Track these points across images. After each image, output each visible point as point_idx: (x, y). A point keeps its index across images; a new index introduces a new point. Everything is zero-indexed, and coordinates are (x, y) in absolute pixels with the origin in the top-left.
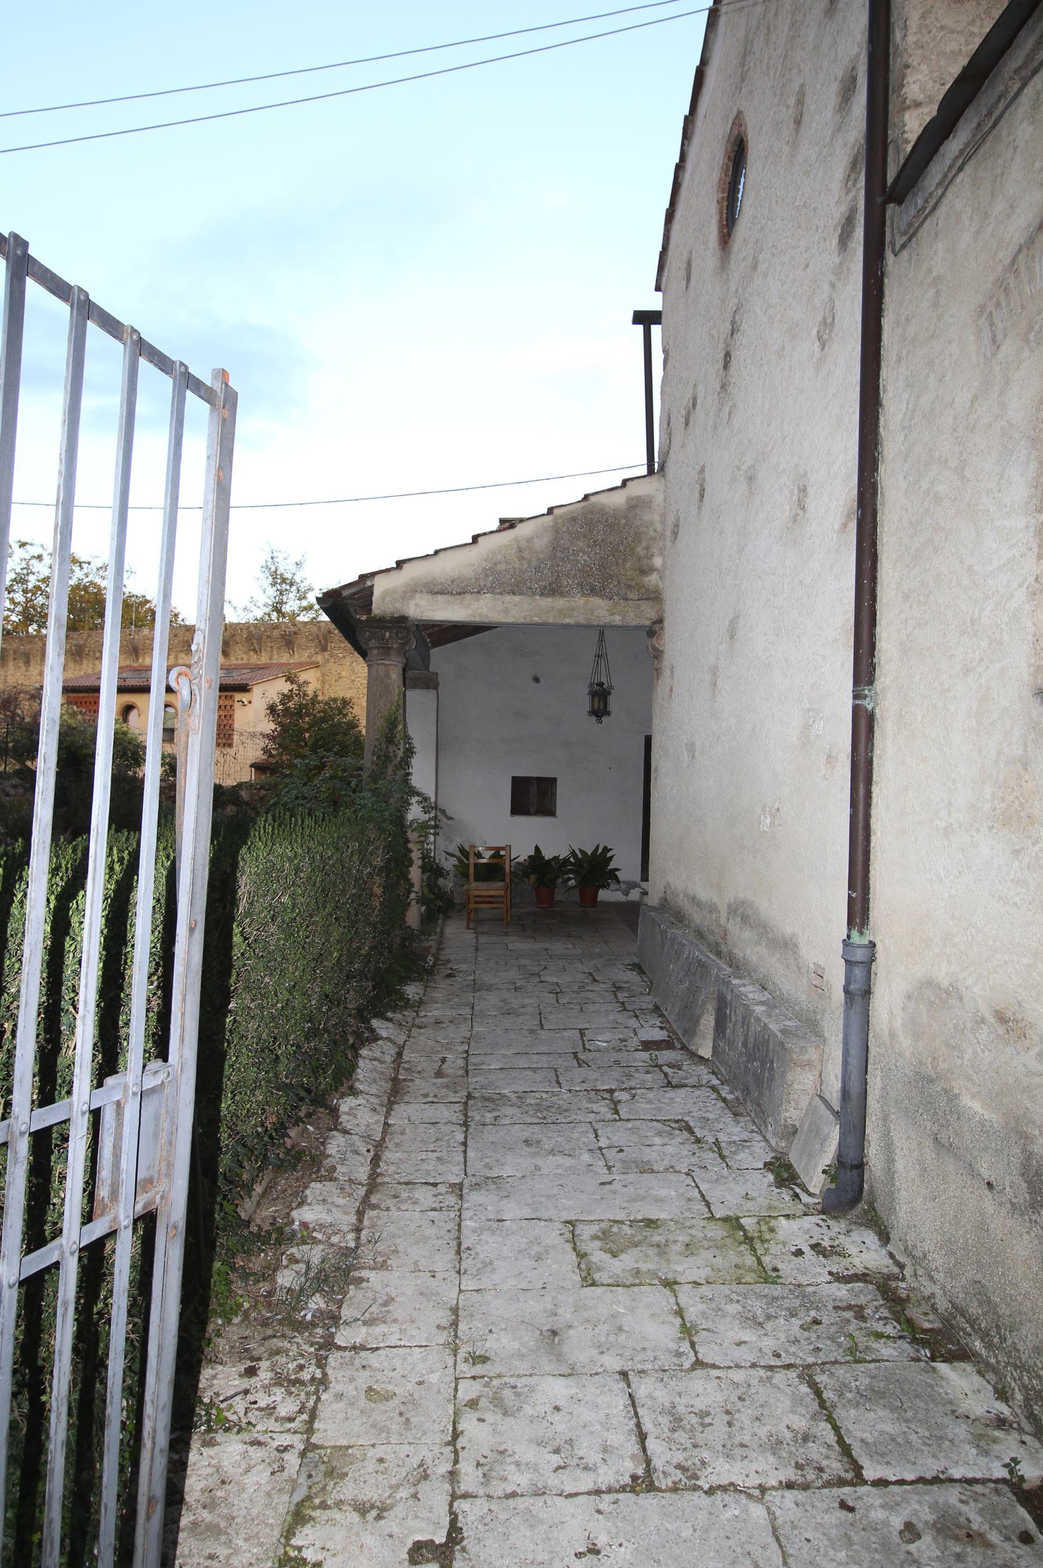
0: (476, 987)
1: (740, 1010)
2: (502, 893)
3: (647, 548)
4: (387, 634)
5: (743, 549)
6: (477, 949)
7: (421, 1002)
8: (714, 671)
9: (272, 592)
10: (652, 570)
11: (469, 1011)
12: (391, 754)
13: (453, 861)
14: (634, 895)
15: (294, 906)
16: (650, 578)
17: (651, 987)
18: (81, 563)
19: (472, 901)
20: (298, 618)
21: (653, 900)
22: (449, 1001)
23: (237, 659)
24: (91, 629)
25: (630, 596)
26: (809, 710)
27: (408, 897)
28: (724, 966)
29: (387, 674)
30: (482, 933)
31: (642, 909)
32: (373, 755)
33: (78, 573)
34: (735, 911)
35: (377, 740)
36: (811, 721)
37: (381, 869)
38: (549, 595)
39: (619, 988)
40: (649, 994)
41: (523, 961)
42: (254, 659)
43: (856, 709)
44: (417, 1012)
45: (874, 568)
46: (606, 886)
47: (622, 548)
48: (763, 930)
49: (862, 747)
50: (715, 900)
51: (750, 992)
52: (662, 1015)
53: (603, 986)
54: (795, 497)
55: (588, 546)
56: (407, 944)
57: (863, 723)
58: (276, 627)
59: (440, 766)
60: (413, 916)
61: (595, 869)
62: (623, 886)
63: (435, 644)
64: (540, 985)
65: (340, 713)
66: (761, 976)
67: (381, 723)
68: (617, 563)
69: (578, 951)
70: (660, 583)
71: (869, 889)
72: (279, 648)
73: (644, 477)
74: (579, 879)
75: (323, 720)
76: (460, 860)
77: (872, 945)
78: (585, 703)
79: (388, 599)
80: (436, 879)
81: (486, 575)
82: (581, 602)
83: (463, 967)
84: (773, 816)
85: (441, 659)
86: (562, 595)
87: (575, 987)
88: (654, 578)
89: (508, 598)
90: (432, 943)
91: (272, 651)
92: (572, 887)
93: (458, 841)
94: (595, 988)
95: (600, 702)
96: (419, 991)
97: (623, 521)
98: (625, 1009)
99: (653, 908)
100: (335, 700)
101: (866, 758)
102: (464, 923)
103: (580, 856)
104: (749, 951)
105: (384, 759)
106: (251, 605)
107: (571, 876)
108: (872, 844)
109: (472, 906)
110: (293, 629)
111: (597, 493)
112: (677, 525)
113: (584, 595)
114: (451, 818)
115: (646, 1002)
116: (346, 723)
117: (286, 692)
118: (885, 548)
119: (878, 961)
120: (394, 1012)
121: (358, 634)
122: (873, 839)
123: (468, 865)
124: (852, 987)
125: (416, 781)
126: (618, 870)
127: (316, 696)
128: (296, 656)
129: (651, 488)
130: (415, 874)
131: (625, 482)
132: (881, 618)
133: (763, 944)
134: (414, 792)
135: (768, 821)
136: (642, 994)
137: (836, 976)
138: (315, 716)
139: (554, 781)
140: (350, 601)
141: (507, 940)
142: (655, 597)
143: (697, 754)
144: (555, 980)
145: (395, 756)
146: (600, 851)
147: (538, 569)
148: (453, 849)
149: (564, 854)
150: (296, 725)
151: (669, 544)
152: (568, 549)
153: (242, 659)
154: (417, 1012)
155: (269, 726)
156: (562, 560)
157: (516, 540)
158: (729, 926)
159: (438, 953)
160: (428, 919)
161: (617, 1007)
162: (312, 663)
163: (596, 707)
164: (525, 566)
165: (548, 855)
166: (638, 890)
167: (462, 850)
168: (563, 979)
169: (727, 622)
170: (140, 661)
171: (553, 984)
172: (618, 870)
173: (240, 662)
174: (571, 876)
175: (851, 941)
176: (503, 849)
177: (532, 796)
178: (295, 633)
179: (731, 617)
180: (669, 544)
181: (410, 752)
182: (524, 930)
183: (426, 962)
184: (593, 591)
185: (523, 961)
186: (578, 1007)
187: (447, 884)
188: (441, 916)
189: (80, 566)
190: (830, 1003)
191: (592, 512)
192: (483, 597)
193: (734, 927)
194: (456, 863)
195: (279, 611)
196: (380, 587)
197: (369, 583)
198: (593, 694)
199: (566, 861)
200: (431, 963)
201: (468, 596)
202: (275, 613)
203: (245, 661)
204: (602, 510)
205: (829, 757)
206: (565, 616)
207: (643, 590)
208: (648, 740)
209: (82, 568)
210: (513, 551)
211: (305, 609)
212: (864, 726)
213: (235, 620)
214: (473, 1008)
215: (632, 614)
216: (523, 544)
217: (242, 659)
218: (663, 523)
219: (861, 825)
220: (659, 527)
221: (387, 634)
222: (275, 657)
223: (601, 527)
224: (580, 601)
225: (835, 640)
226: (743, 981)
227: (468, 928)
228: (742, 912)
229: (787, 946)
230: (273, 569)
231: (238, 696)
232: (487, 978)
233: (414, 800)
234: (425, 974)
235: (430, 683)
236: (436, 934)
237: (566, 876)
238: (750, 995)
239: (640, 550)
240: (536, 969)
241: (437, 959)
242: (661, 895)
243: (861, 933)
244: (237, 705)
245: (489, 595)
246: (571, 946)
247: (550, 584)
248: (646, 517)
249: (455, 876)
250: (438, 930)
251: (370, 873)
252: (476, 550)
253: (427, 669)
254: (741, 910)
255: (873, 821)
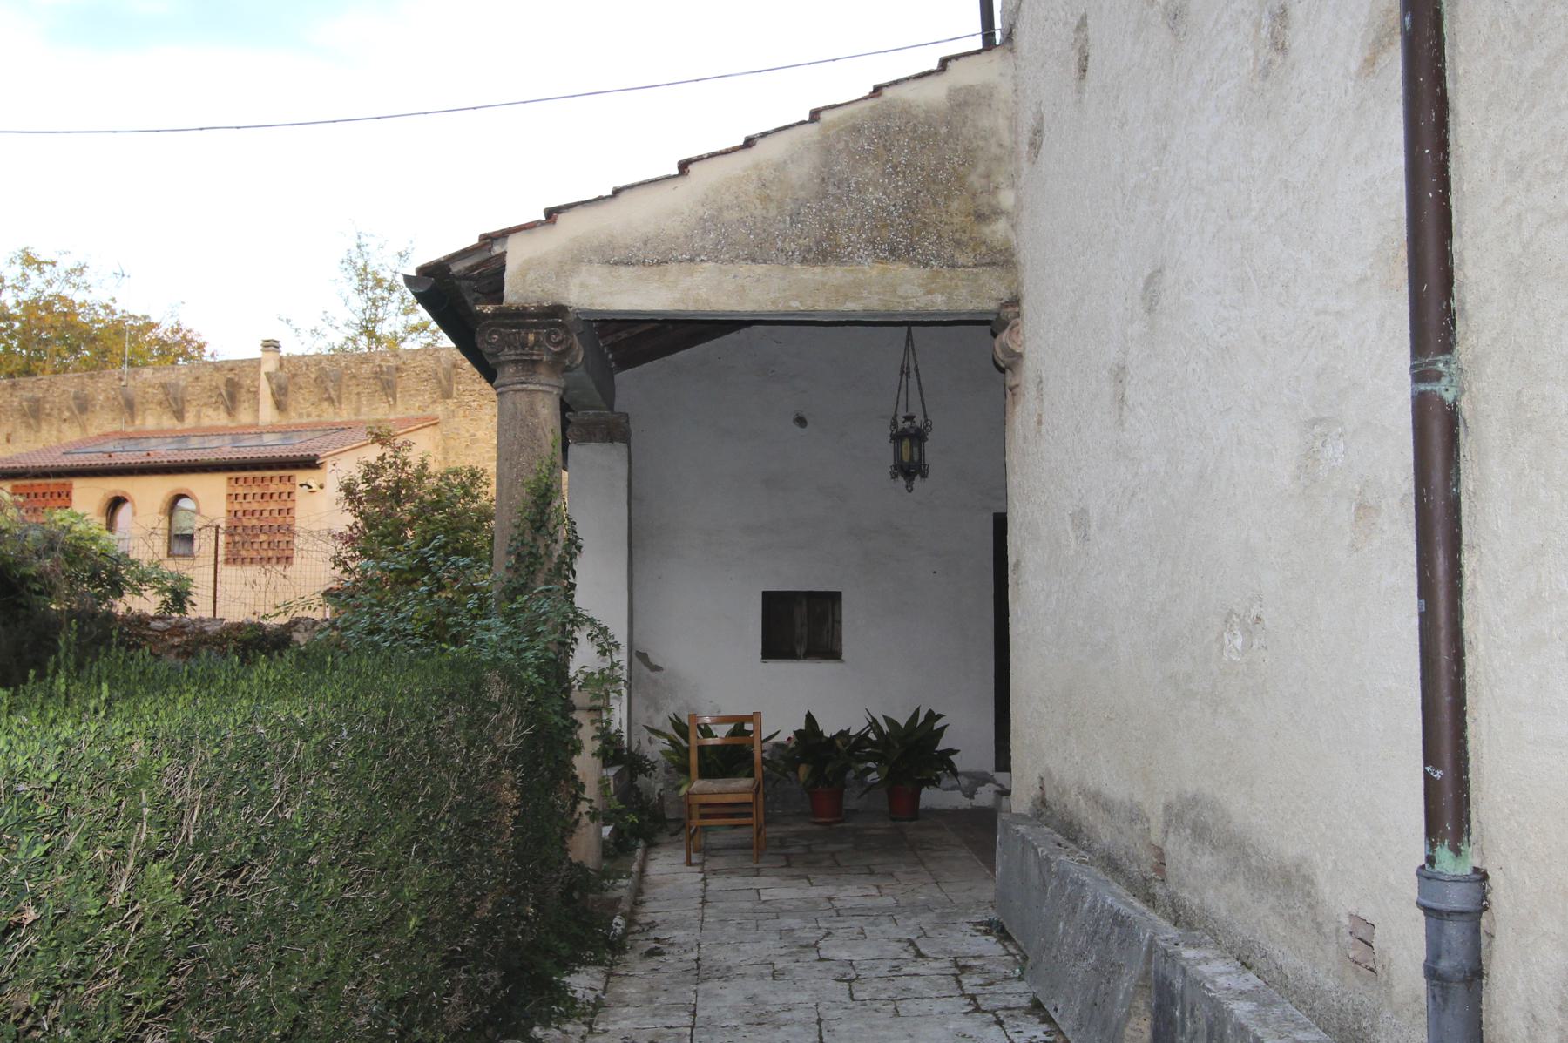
0: (700, 972)
1: (1203, 1012)
2: (749, 798)
3: (988, 176)
4: (531, 337)
5: (1165, 146)
6: (704, 902)
7: (598, 1005)
8: (1119, 374)
9: (359, 302)
10: (997, 212)
11: (688, 1020)
12: (542, 551)
13: (662, 744)
14: (985, 796)
15: (314, 825)
16: (993, 227)
17: (1025, 965)
18: (40, 263)
19: (695, 813)
20: (403, 345)
21: (1022, 799)
22: (651, 1001)
23: (300, 415)
24: (56, 372)
25: (961, 260)
26: (1315, 422)
27: (573, 809)
28: (1164, 923)
29: (532, 410)
30: (715, 872)
31: (1002, 817)
32: (509, 553)
33: (36, 281)
34: (1180, 817)
35: (517, 527)
36: (1318, 443)
37: (515, 757)
38: (815, 262)
39: (964, 969)
40: (1020, 979)
41: (788, 922)
42: (329, 415)
43: (1422, 406)
44: (589, 1024)
45: (1442, 125)
46: (934, 782)
47: (942, 176)
48: (1238, 852)
49: (1437, 477)
50: (1138, 798)
51: (1216, 972)
52: (1047, 1019)
53: (933, 964)
54: (1264, 33)
55: (884, 174)
56: (576, 895)
57: (1436, 429)
58: (365, 359)
59: (636, 575)
60: (587, 842)
61: (912, 751)
62: (964, 781)
63: (626, 362)
64: (820, 966)
65: (467, 494)
66: (1239, 941)
67: (521, 496)
68: (935, 203)
69: (888, 901)
70: (1012, 236)
71: (1466, 760)
72: (371, 395)
73: (978, 52)
74: (886, 770)
75: (437, 506)
76: (673, 743)
77: (1481, 876)
78: (885, 453)
79: (531, 276)
80: (633, 777)
81: (705, 231)
82: (874, 272)
83: (679, 935)
84: (1248, 632)
85: (633, 386)
86: (839, 260)
87: (884, 969)
88: (1000, 228)
89: (744, 269)
90: (623, 892)
91: (359, 400)
92: (872, 786)
93: (671, 707)
94: (921, 970)
95: (910, 458)
96: (595, 984)
97: (943, 130)
98: (977, 1009)
99: (1023, 818)
100: (457, 473)
101: (1447, 498)
102: (683, 853)
103: (886, 729)
104: (1210, 894)
105: (527, 560)
106: (325, 325)
107: (871, 765)
108: (1469, 672)
109: (696, 822)
110: (394, 362)
111: (896, 83)
112: (1038, 131)
113: (878, 260)
114: (657, 668)
115: (1017, 993)
116: (479, 511)
117: (373, 460)
118: (1463, 84)
119: (1494, 908)
120: (546, 1025)
121: (478, 339)
122: (1469, 659)
123: (687, 750)
124: (1444, 965)
125: (583, 600)
126: (955, 752)
127: (424, 466)
128: (400, 407)
129: (988, 71)
130: (586, 766)
131: (944, 63)
132: (1460, 222)
133: (1241, 879)
134: (578, 620)
135: (1238, 642)
136: (1007, 978)
137: (1406, 944)
138: (421, 499)
139: (834, 598)
140: (464, 284)
141: (759, 882)
142: (1003, 260)
143: (1093, 530)
144: (845, 955)
145: (549, 555)
146: (921, 719)
147: (795, 217)
148: (662, 722)
149: (857, 726)
150: (388, 516)
151: (1025, 165)
152: (847, 180)
153: (309, 415)
154: (589, 1024)
155: (345, 520)
156: (838, 199)
157: (756, 166)
158: (1168, 847)
159: (633, 912)
160: (618, 848)
161: (963, 1004)
162: (426, 419)
163: (906, 458)
164: (773, 213)
165: (828, 728)
166: (990, 787)
167: (679, 726)
168: (863, 953)
169: (1140, 284)
170: (138, 422)
171: (842, 963)
172: (955, 752)
173: (305, 420)
174: (871, 765)
175: (1437, 868)
176: (749, 719)
177: (799, 626)
178: (398, 369)
179: (1147, 272)
180: (1025, 165)
181: (573, 546)
182: (789, 866)
183: (610, 928)
184: (894, 253)
185: (788, 922)
186: (891, 1007)
187: (653, 785)
188: (641, 843)
189: (39, 269)
190: (1388, 994)
191: (888, 116)
192: (699, 267)
193: (1178, 849)
194: (669, 748)
195: (371, 334)
196: (516, 255)
197: (497, 250)
198: (897, 437)
199: (861, 737)
200: (619, 930)
201: (674, 267)
202: (364, 339)
203: (314, 419)
204: (906, 111)
205: (1360, 507)
206: (846, 297)
207: (984, 249)
208: (1000, 524)
209: (41, 271)
210: (751, 187)
211: (415, 329)
212: (1438, 435)
213: (297, 350)
214: (694, 1014)
215: (964, 292)
216: (768, 174)
217: (309, 415)
218: (1014, 129)
219: (1443, 634)
220: (1007, 139)
221: (531, 337)
222: (364, 409)
223: (904, 141)
224: (871, 270)
225: (1363, 280)
226: (1202, 953)
227: (689, 863)
228: (1194, 819)
229: (1289, 882)
230: (360, 264)
231: (301, 476)
232: (722, 956)
233: (582, 634)
234: (606, 948)
235: (614, 431)
236: (629, 876)
237: (862, 766)
238: (1221, 981)
239: (975, 180)
240: (809, 935)
241: (631, 922)
242: (1035, 792)
243: (1457, 852)
244: (300, 492)
245: (710, 265)
246: (874, 891)
247: (818, 243)
248: (985, 121)
249: (667, 772)
250: (635, 868)
251: (493, 764)
252: (684, 185)
253: (611, 408)
254: (1192, 815)
255: (1467, 624)
